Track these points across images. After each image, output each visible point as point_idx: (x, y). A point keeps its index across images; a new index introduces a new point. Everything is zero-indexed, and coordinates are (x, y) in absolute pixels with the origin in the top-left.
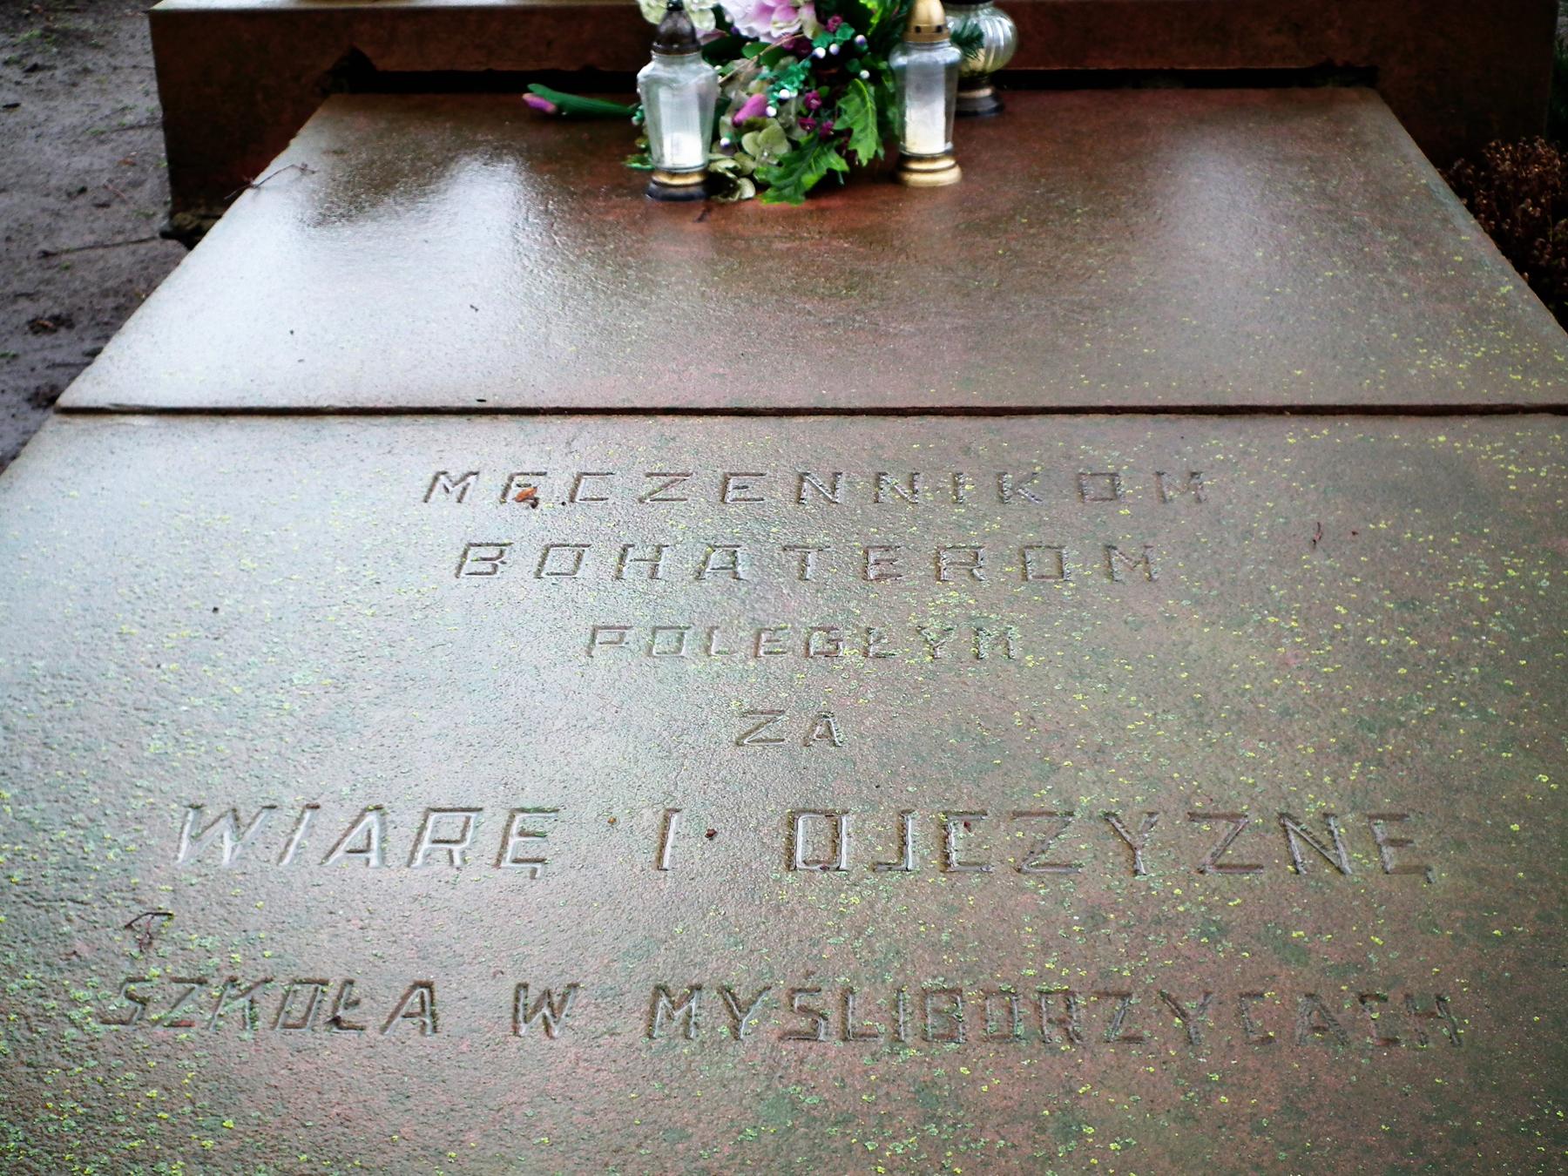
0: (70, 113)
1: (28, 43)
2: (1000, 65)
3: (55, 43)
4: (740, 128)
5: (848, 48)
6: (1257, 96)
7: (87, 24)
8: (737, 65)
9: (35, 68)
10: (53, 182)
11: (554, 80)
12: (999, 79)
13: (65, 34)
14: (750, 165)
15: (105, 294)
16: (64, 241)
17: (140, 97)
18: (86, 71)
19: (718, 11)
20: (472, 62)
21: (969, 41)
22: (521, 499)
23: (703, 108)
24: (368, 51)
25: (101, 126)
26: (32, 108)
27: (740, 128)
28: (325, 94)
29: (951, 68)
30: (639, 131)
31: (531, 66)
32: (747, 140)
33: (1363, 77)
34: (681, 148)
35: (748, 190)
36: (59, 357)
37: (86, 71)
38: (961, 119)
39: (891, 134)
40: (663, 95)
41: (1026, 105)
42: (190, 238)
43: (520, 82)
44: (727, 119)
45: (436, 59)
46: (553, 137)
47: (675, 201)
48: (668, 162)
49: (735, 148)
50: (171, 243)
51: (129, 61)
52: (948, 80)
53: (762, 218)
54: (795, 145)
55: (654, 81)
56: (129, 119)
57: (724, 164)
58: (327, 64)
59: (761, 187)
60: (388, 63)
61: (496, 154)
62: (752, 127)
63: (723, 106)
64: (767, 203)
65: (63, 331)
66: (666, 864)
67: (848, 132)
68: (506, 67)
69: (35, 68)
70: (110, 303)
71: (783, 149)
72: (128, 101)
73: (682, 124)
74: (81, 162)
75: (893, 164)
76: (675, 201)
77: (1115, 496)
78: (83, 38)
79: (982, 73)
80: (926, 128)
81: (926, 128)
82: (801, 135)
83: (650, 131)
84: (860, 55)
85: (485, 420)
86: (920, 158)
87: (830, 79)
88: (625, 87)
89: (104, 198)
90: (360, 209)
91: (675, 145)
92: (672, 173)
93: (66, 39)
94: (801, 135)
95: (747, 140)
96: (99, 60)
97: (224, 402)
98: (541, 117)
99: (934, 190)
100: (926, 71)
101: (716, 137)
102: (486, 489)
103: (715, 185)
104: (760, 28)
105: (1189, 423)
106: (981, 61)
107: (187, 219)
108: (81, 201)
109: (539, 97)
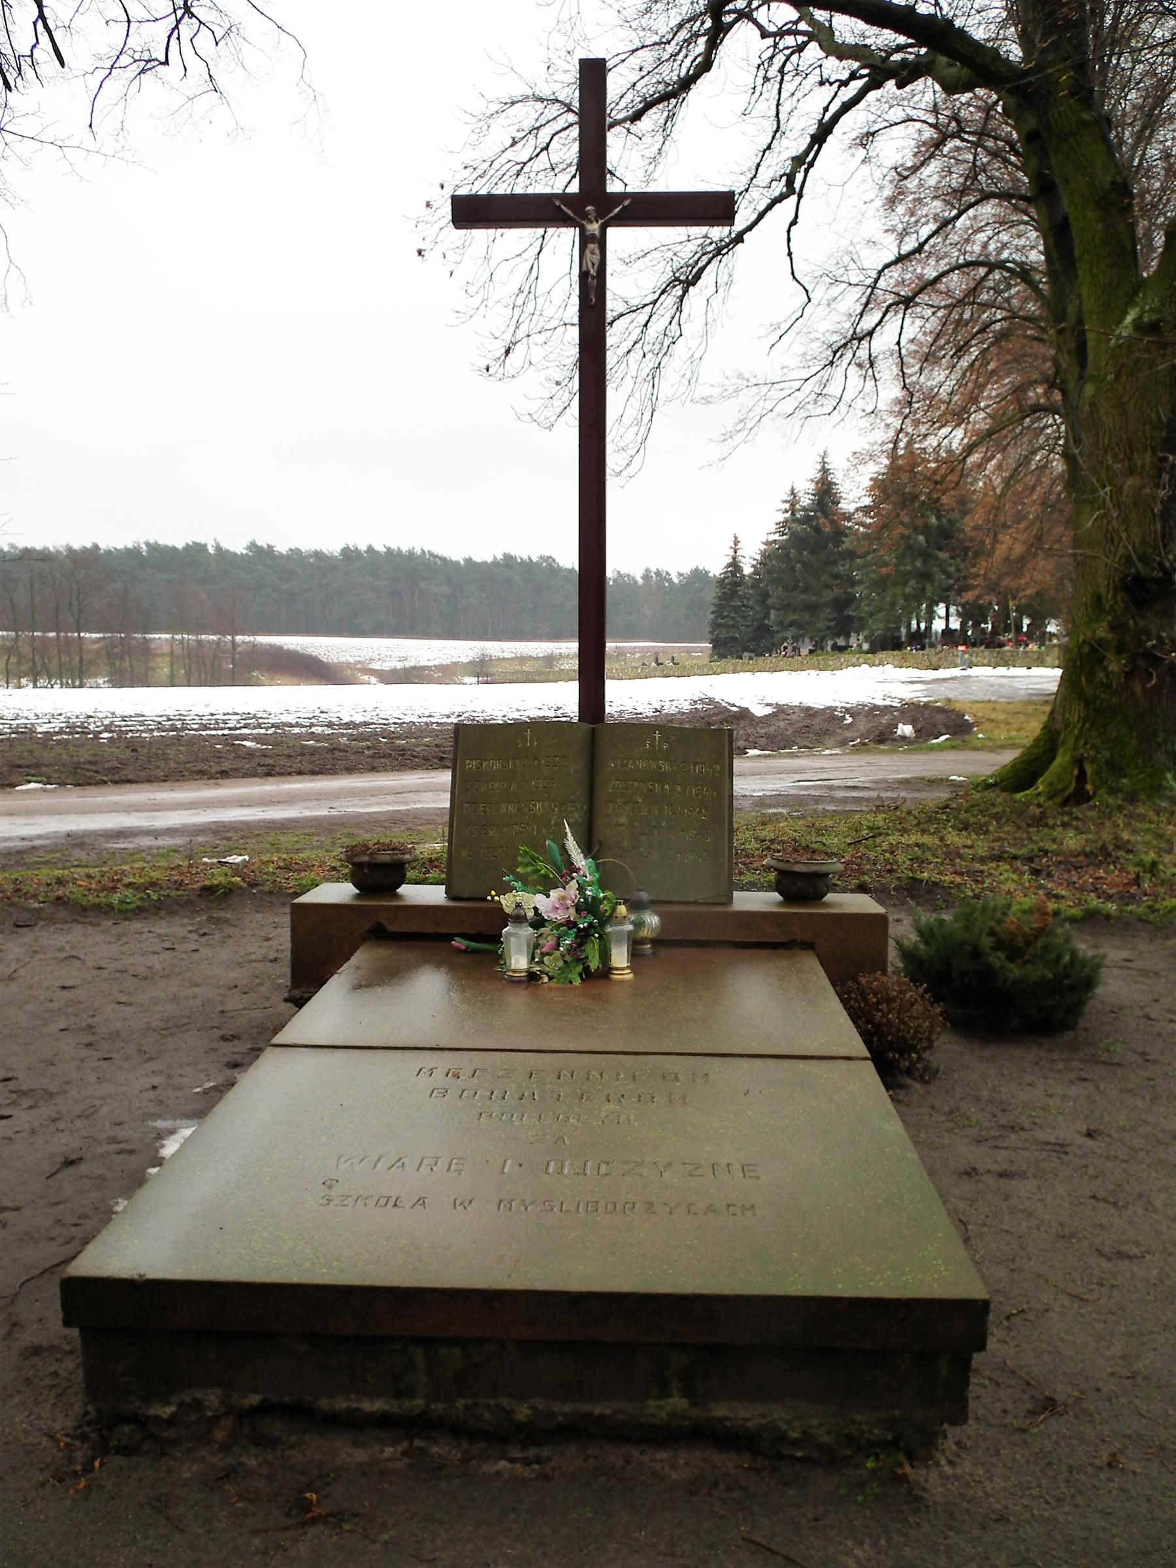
0: (224, 954)
1: (200, 923)
2: (654, 935)
3: (213, 923)
4: (543, 955)
5: (591, 925)
6: (763, 952)
7: (228, 915)
8: (543, 930)
9: (205, 934)
10: (221, 983)
11: (464, 936)
12: (654, 942)
13: (218, 919)
14: (547, 969)
15: (253, 1027)
16: (229, 1006)
17: (284, 938)
18: (230, 936)
19: (536, 909)
20: (429, 929)
21: (639, 925)
22: (454, 1075)
23: (528, 947)
24: (384, 923)
25: (240, 960)
26: (205, 952)
27: (543, 955)
28: (364, 940)
29: (629, 932)
30: (501, 957)
31: (454, 931)
32: (546, 959)
33: (810, 946)
34: (519, 962)
35: (546, 979)
36: (237, 1050)
37: (230, 936)
38: (635, 955)
39: (605, 956)
40: (513, 940)
41: (665, 953)
42: (299, 1003)
43: (449, 937)
44: (538, 951)
45: (415, 927)
46: (462, 959)
47: (514, 982)
48: (513, 967)
49: (541, 962)
50: (290, 1005)
51: (249, 932)
52: (629, 938)
53: (551, 989)
54: (566, 962)
55: (509, 934)
56: (253, 957)
57: (536, 969)
58: (367, 927)
59: (551, 978)
60: (392, 928)
61: (439, 965)
62: (547, 954)
63: (536, 946)
64: (553, 984)
65: (236, 1041)
66: (506, 1171)
67: (587, 958)
68: (445, 931)
69: (205, 934)
70: (256, 1031)
71: (561, 964)
72: (251, 950)
73: (519, 952)
74: (233, 975)
75: (606, 971)
76: (514, 982)
77: (676, 1079)
78: (227, 921)
79: (646, 938)
80: (620, 957)
81: (620, 957)
82: (568, 958)
83: (506, 956)
84: (595, 928)
85: (439, 1052)
86: (617, 969)
87: (583, 936)
88: (496, 939)
89: (246, 990)
90: (384, 982)
91: (517, 960)
92: (515, 971)
93: (218, 921)
94: (568, 958)
95: (546, 959)
96: (235, 931)
97: (337, 1044)
98: (459, 951)
99: (622, 982)
100: (620, 933)
101: (533, 958)
102: (439, 1074)
103: (532, 977)
104: (553, 916)
105: (707, 1059)
106: (645, 933)
107: (297, 993)
108: (235, 991)
109: (459, 943)
